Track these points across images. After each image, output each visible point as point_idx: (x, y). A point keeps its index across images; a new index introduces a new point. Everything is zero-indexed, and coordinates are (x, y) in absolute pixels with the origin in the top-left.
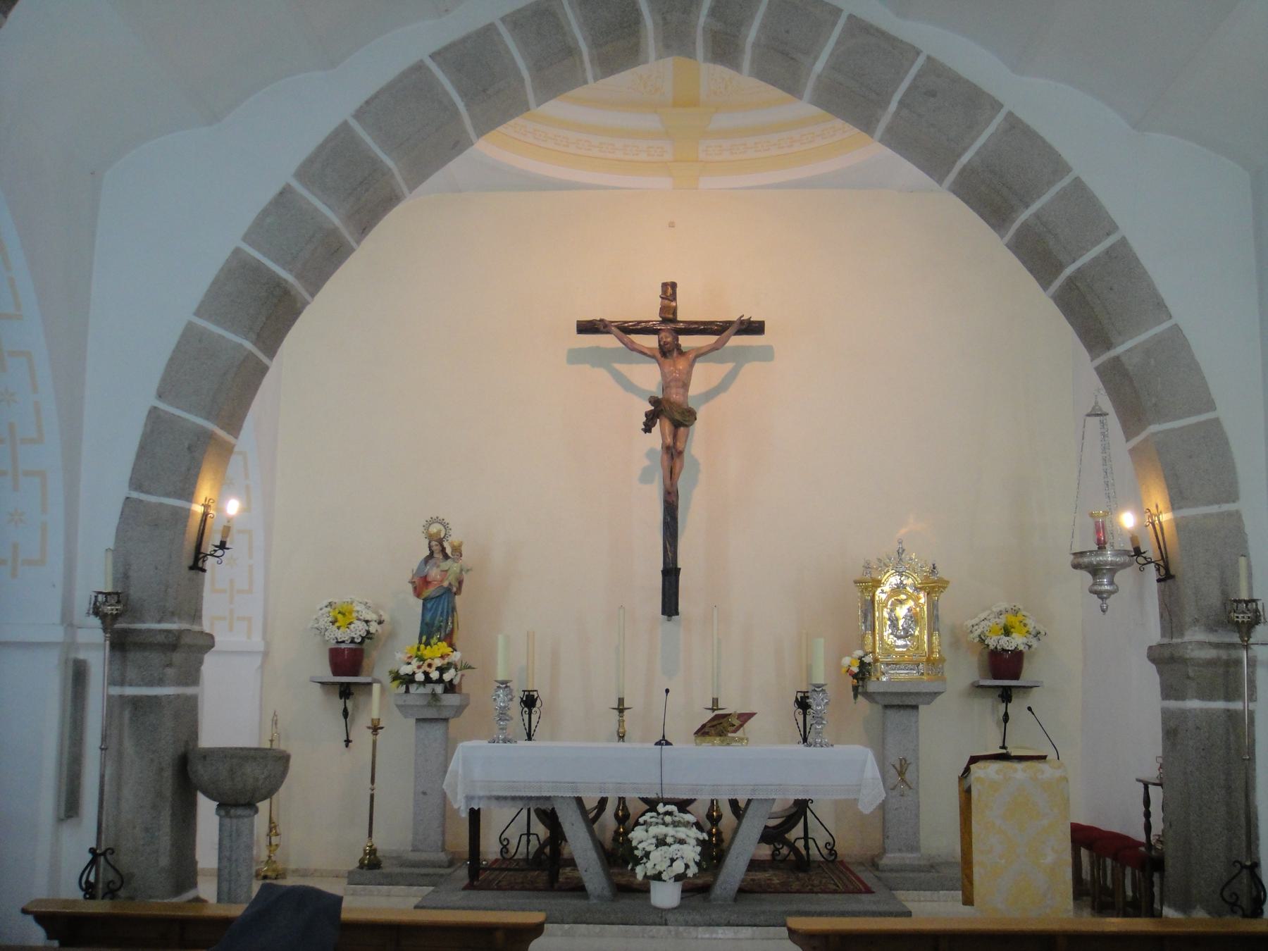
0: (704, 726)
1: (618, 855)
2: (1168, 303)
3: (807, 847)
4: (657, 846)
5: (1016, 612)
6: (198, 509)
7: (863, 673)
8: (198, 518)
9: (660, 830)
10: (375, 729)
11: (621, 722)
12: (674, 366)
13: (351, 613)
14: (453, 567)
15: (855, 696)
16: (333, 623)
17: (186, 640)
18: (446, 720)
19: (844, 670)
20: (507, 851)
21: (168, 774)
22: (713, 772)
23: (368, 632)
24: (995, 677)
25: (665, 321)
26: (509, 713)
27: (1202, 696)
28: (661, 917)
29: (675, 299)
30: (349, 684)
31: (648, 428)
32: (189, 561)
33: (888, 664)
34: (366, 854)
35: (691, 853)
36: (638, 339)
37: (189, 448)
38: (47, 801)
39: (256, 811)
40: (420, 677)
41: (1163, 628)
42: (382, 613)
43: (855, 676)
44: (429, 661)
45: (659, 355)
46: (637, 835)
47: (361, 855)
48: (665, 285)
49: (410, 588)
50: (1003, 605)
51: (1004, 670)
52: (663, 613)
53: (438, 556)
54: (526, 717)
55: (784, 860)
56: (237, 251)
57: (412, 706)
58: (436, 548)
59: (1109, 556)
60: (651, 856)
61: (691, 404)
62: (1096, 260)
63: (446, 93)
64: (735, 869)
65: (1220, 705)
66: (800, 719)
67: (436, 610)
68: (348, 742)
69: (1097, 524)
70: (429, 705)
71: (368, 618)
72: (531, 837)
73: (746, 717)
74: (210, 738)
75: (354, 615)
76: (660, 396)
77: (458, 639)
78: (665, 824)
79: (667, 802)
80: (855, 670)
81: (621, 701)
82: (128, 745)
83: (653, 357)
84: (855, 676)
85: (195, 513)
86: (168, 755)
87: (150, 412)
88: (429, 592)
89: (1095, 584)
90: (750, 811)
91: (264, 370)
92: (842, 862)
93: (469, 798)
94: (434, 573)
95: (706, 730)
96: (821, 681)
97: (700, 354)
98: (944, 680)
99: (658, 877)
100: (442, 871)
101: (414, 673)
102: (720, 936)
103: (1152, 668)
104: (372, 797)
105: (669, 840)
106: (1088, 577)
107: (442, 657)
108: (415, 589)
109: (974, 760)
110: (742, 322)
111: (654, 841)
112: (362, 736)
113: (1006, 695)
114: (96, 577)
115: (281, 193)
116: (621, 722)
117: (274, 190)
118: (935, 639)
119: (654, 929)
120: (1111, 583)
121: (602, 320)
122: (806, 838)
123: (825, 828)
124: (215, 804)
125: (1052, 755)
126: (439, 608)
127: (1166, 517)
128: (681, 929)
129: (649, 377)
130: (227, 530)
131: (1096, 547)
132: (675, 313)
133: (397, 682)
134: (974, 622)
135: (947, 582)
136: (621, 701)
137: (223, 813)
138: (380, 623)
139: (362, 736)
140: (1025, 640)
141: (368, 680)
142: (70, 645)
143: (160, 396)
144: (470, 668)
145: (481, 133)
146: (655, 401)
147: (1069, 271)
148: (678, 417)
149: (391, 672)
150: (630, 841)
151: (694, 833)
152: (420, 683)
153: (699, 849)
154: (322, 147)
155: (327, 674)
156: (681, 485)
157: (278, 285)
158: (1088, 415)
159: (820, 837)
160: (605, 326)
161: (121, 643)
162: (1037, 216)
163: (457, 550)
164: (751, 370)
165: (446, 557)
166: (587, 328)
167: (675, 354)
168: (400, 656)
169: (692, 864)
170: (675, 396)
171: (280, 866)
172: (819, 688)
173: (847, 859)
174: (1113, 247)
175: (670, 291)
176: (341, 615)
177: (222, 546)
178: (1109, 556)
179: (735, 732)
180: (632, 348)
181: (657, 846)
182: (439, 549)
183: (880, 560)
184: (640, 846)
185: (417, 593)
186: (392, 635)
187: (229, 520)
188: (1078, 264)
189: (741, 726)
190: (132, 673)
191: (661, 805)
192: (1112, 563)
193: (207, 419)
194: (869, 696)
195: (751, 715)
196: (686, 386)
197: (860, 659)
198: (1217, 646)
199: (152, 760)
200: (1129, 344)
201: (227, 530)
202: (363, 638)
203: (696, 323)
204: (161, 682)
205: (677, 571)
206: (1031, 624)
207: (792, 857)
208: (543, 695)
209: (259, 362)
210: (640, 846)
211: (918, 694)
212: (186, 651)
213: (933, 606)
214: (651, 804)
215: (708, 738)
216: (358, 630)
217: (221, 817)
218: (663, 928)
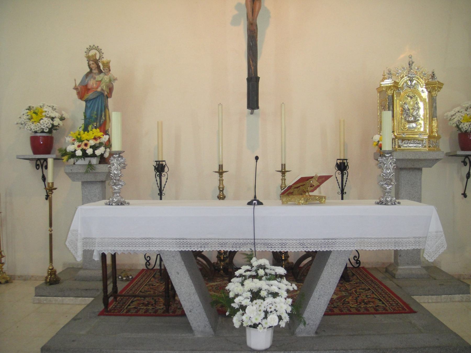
4: (252, 301)
11: (221, 181)
19: (375, 144)
20: (150, 264)
24: (463, 149)
34: (48, 275)
35: (284, 305)
40: (79, 153)
42: (63, 112)
44: (86, 142)
52: (249, 107)
53: (95, 71)
54: (158, 178)
57: (77, 173)
58: (94, 66)
66: (339, 177)
71: (53, 115)
75: (44, 114)
81: (221, 167)
88: (89, 95)
92: (363, 268)
94: (92, 83)
101: (75, 150)
104: (51, 236)
105: (263, 293)
107: (95, 139)
108: (78, 93)
111: (249, 295)
116: (221, 181)
118: (435, 124)
134: (452, 113)
136: (221, 167)
152: (79, 157)
153: (290, 301)
155: (29, 152)
156: (259, 22)
163: (107, 65)
165: (100, 72)
173: (367, 266)
176: (34, 113)
179: (312, 191)
181: (252, 301)
182: (97, 66)
185: (81, 96)
189: (318, 186)
205: (257, 79)
208: (169, 163)
216: (45, 123)
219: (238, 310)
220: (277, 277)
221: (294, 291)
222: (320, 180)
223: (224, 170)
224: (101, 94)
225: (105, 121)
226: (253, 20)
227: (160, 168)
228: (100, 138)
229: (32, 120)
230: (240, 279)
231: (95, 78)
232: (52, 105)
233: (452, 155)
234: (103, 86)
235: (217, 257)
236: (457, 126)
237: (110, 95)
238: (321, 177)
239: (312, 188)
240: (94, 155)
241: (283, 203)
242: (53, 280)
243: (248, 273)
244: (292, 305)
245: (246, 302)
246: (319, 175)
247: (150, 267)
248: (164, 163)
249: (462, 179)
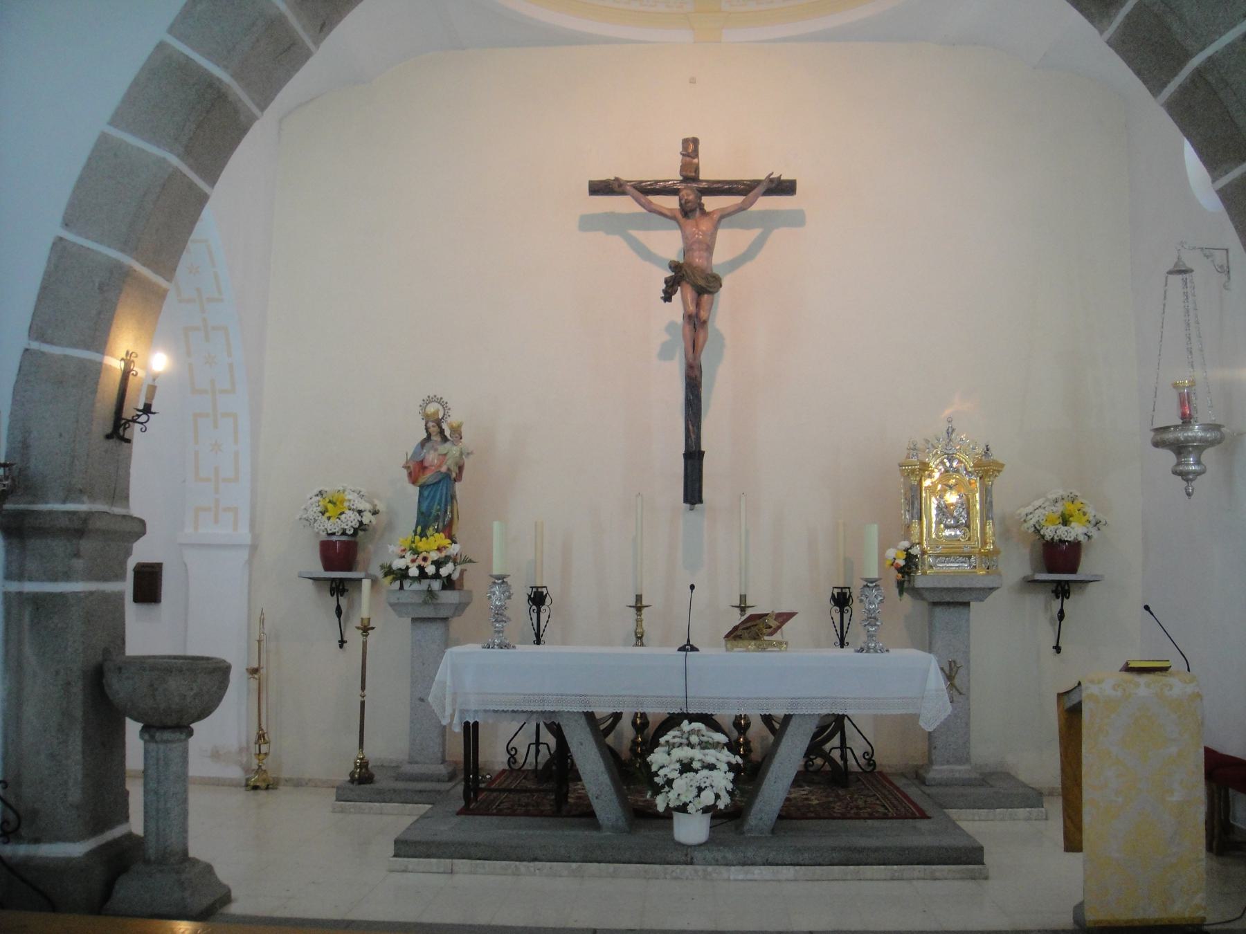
0: (736, 628)
3: (844, 757)
4: (681, 773)
6: (115, 363)
7: (909, 565)
8: (118, 377)
10: (366, 629)
11: (639, 622)
12: (697, 226)
13: (342, 502)
14: (453, 450)
15: (901, 593)
18: (445, 619)
19: (889, 562)
20: (516, 761)
21: (77, 689)
22: (745, 683)
23: (361, 523)
24: (1051, 570)
25: (686, 179)
26: (507, 613)
28: (687, 855)
29: (697, 156)
30: (342, 580)
31: (667, 297)
33: (937, 556)
34: (356, 767)
35: (722, 780)
36: (657, 200)
37: (100, 288)
39: (190, 733)
40: (414, 572)
42: (376, 502)
43: (901, 570)
44: (424, 554)
45: (680, 216)
46: (657, 758)
47: (352, 767)
48: (686, 142)
50: (1060, 492)
51: (1058, 564)
52: (686, 501)
54: (535, 616)
55: (818, 771)
56: (161, 46)
58: (434, 430)
59: (1196, 431)
60: (675, 785)
61: (715, 271)
67: (434, 497)
69: (1181, 395)
70: (425, 603)
71: (361, 507)
72: (541, 747)
73: (785, 617)
75: (346, 504)
76: (681, 261)
78: (691, 746)
79: (693, 718)
80: (902, 563)
81: (639, 598)
82: (28, 651)
83: (673, 218)
84: (901, 570)
85: (110, 368)
87: (54, 244)
88: (427, 477)
89: (1179, 464)
90: (791, 729)
91: (203, 199)
92: (880, 773)
94: (431, 457)
95: (739, 633)
96: (874, 574)
97: (725, 215)
99: (683, 808)
100: (439, 786)
101: (408, 568)
102: (756, 877)
104: (363, 704)
105: (696, 765)
106: (1169, 457)
107: (439, 549)
108: (410, 474)
111: (678, 766)
112: (354, 636)
113: (1062, 591)
116: (639, 622)
120: (1198, 462)
121: (617, 179)
122: (843, 746)
123: (868, 738)
124: (140, 726)
125: (1176, 663)
126: (438, 494)
128: (710, 868)
130: (152, 390)
131: (1180, 422)
132: (697, 170)
133: (390, 578)
134: (1030, 509)
135: (1003, 465)
136: (639, 598)
137: (147, 737)
138: (375, 513)
139: (354, 636)
140: (1085, 530)
143: (66, 224)
144: (471, 561)
146: (675, 267)
147: (1196, 62)
148: (701, 282)
149: (382, 567)
150: (648, 766)
151: (725, 756)
152: (414, 579)
153: (731, 775)
155: (319, 571)
156: (705, 359)
157: (211, 85)
158: (1170, 272)
159: (857, 745)
160: (620, 185)
163: (457, 431)
164: (779, 235)
165: (445, 439)
166: (600, 188)
167: (698, 213)
168: (394, 549)
169: (723, 794)
170: (698, 260)
171: (271, 775)
173: (886, 770)
175: (691, 147)
176: (331, 503)
177: (147, 409)
178: (1196, 431)
179: (771, 634)
180: (652, 210)
181: (681, 773)
182: (437, 430)
183: (927, 441)
184: (661, 773)
185: (413, 479)
186: (390, 526)
187: (155, 377)
188: (1209, 51)
189: (779, 627)
190: (32, 566)
191: (686, 722)
192: (1201, 440)
193: (123, 251)
194: (917, 593)
196: (709, 248)
197: (907, 550)
199: (57, 673)
201: (152, 390)
202: (356, 530)
203: (719, 182)
204: (67, 576)
205: (701, 454)
207: (828, 767)
209: (191, 186)
210: (661, 773)
215: (741, 643)
216: (350, 520)
217: (146, 742)
219: (663, 786)
220: (716, 746)
221: (738, 764)
222: (781, 619)
223: (644, 603)
224: (447, 476)
225: (452, 519)
226: (695, 359)
227: (538, 599)
228: (445, 548)
229: (327, 514)
230: (666, 749)
231: (436, 450)
232: (359, 488)
233: (1030, 583)
234: (450, 463)
235: (631, 750)
236: (1037, 531)
237: (459, 477)
238: (779, 615)
239: (769, 631)
240: (437, 576)
241: (727, 650)
242: (363, 776)
243: (677, 740)
244: (733, 782)
246: (777, 611)
247: (516, 767)
248: (544, 591)
249: (1052, 624)
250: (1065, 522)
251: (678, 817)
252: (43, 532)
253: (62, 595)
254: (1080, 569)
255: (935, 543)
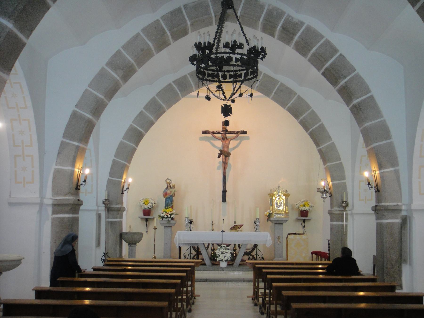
1: (213, 258)
2: (332, 137)
3: (256, 257)
5: (307, 201)
7: (270, 215)
8: (122, 183)
9: (222, 250)
10: (155, 229)
11: (213, 227)
14: (173, 190)
16: (144, 203)
17: (121, 209)
18: (171, 227)
24: (302, 217)
27: (337, 221)
31: (219, 157)
32: (121, 192)
35: (229, 255)
36: (217, 135)
38: (94, 243)
40: (166, 216)
41: (376, 201)
43: (268, 216)
49: (162, 195)
50: (304, 200)
51: (304, 215)
53: (169, 188)
56: (131, 125)
58: (169, 186)
61: (230, 151)
62: (317, 128)
63: (176, 90)
64: (238, 260)
65: (340, 223)
68: (147, 232)
73: (241, 226)
74: (124, 230)
77: (174, 208)
80: (268, 215)
81: (213, 222)
82: (110, 231)
83: (220, 140)
84: (268, 216)
86: (118, 234)
88: (167, 196)
93: (179, 244)
94: (168, 192)
96: (258, 218)
98: (289, 217)
99: (222, 260)
103: (329, 215)
109: (289, 234)
110: (242, 131)
113: (304, 221)
114: (103, 196)
115: (140, 112)
116: (213, 227)
117: (139, 111)
118: (287, 208)
119: (221, 272)
122: (256, 255)
126: (169, 200)
127: (331, 183)
129: (219, 144)
136: (213, 222)
141: (152, 217)
142: (98, 210)
143: (115, 156)
145: (183, 97)
154: (149, 102)
155: (143, 217)
156: (227, 170)
161: (109, 210)
162: (304, 118)
163: (174, 186)
164: (244, 142)
165: (171, 188)
166: (204, 132)
168: (161, 212)
170: (226, 149)
172: (258, 219)
174: (320, 125)
176: (146, 201)
180: (215, 137)
182: (169, 186)
185: (164, 196)
186: (157, 206)
188: (312, 129)
195: (242, 225)
196: (228, 147)
198: (340, 211)
200: (323, 146)
201: (129, 185)
204: (116, 218)
206: (310, 204)
208: (194, 221)
211: (282, 221)
212: (120, 210)
213: (286, 200)
214: (219, 245)
216: (150, 205)
218: (223, 272)
237: (174, 196)
245: (220, 254)
250: (304, 206)
251: (221, 262)
252: (112, 210)
253: (116, 221)
254: (308, 216)
255: (275, 211)
